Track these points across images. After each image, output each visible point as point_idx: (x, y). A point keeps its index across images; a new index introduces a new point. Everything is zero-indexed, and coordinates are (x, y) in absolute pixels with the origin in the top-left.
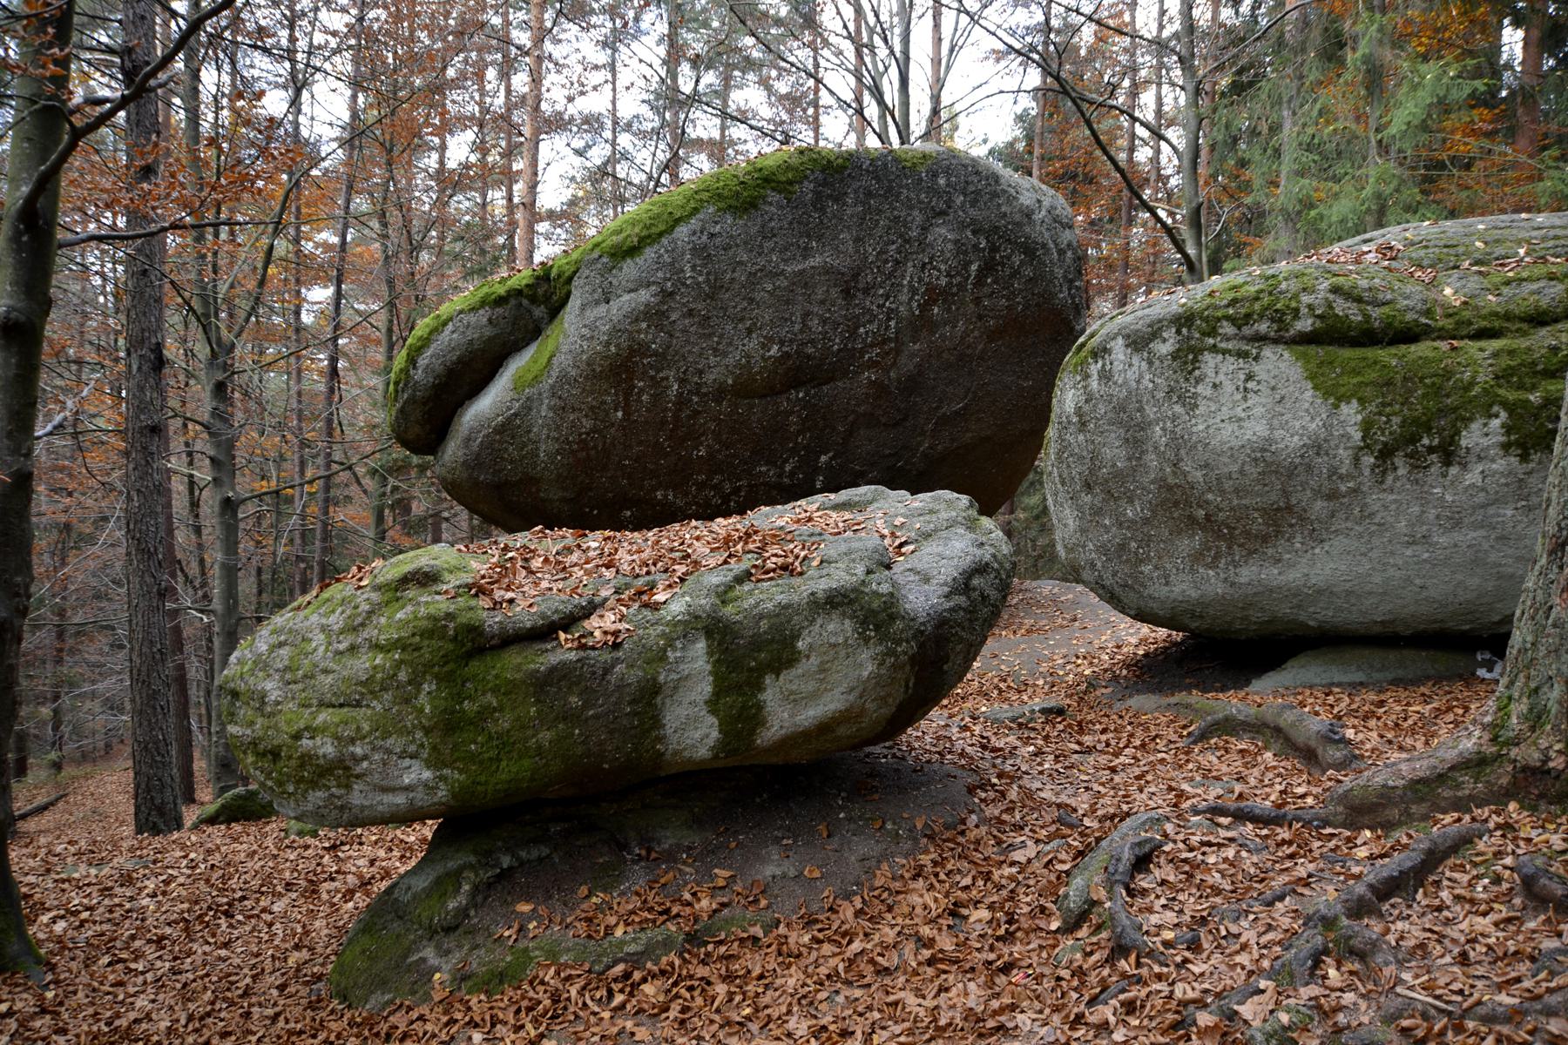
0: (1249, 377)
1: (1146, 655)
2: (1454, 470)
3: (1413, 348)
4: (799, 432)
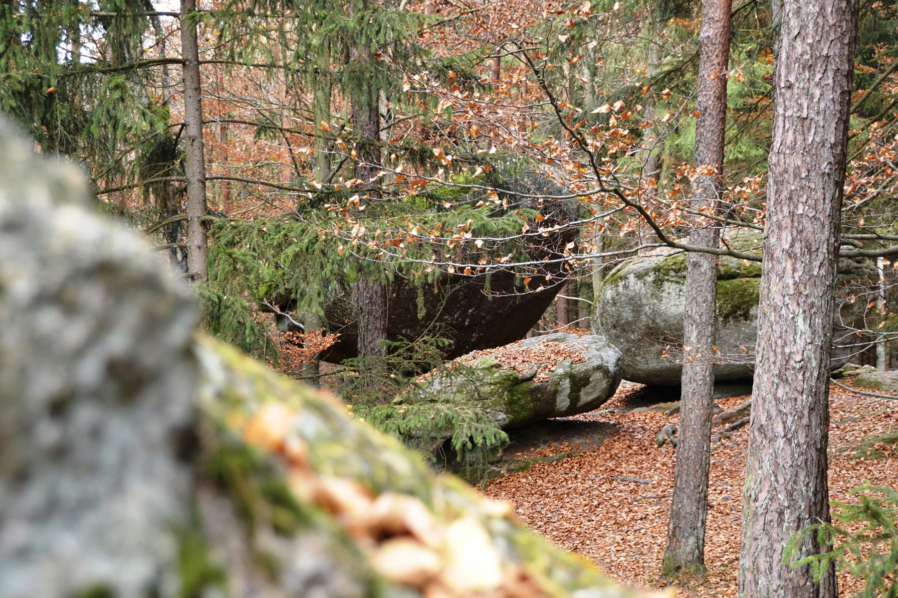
0: (680, 291)
1: (627, 397)
2: (748, 322)
3: (734, 281)
4: (463, 299)
